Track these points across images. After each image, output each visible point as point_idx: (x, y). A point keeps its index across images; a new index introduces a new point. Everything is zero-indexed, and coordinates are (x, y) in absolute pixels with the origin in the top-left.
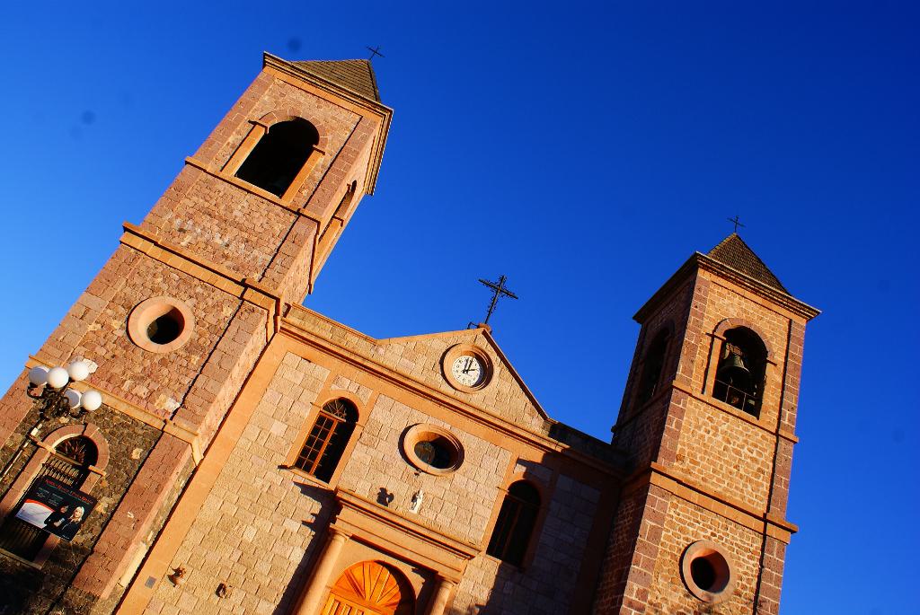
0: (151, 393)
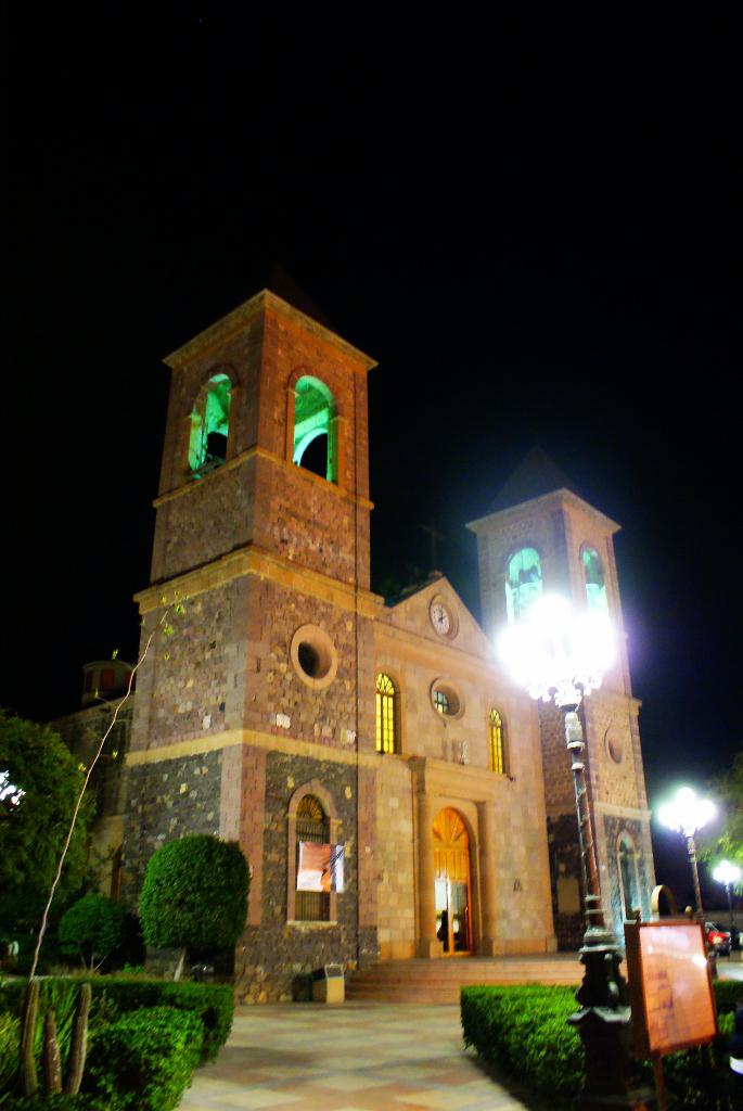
0: (334, 731)
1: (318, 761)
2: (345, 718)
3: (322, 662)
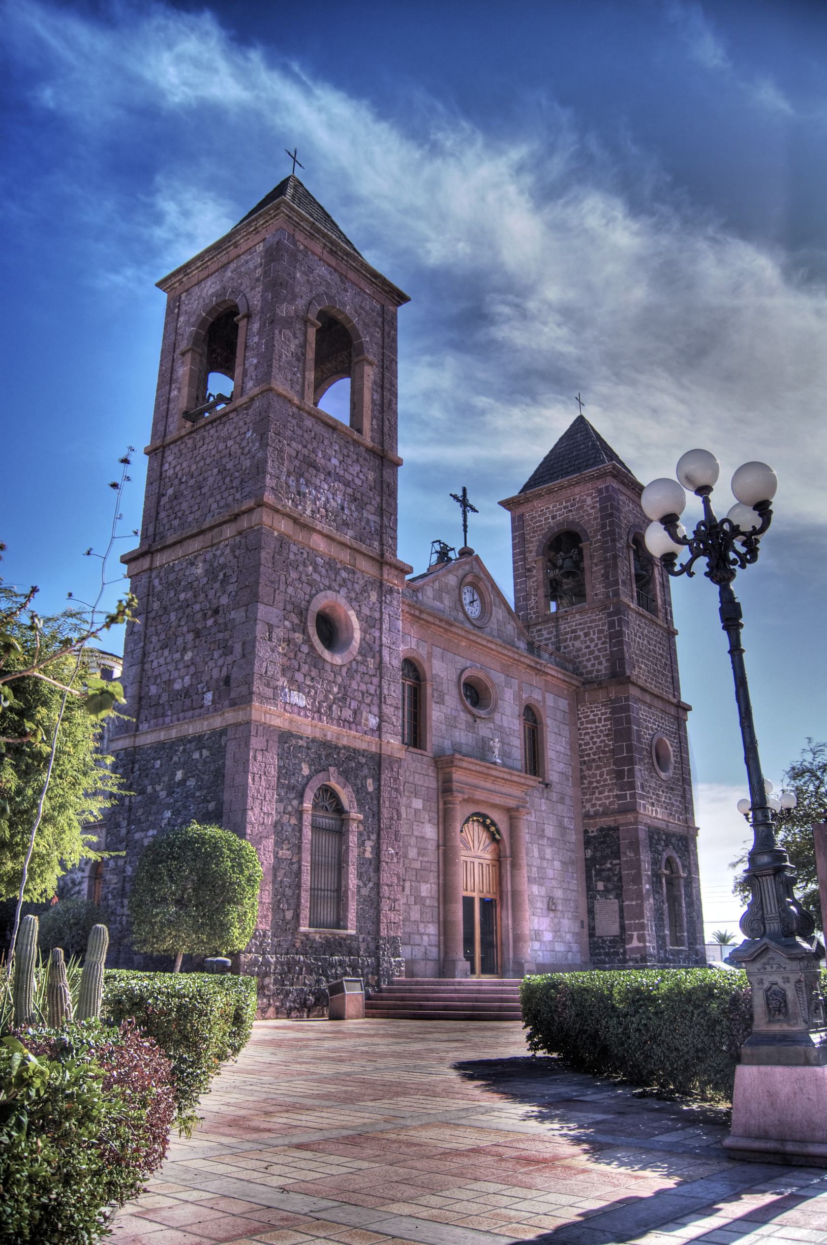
0: (355, 713)
1: (336, 747)
2: (368, 701)
3: (343, 636)
